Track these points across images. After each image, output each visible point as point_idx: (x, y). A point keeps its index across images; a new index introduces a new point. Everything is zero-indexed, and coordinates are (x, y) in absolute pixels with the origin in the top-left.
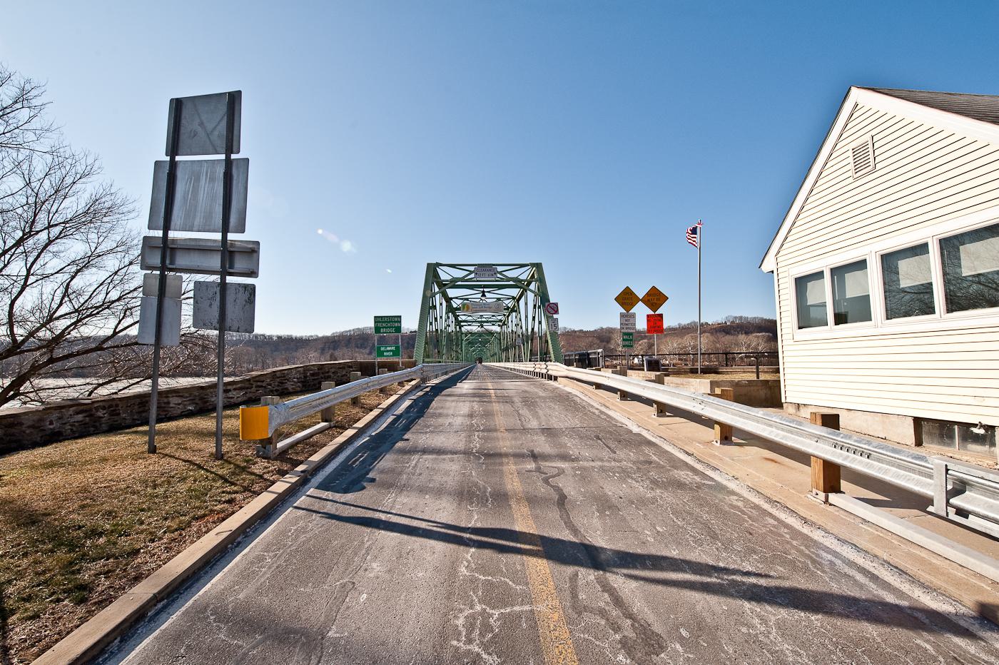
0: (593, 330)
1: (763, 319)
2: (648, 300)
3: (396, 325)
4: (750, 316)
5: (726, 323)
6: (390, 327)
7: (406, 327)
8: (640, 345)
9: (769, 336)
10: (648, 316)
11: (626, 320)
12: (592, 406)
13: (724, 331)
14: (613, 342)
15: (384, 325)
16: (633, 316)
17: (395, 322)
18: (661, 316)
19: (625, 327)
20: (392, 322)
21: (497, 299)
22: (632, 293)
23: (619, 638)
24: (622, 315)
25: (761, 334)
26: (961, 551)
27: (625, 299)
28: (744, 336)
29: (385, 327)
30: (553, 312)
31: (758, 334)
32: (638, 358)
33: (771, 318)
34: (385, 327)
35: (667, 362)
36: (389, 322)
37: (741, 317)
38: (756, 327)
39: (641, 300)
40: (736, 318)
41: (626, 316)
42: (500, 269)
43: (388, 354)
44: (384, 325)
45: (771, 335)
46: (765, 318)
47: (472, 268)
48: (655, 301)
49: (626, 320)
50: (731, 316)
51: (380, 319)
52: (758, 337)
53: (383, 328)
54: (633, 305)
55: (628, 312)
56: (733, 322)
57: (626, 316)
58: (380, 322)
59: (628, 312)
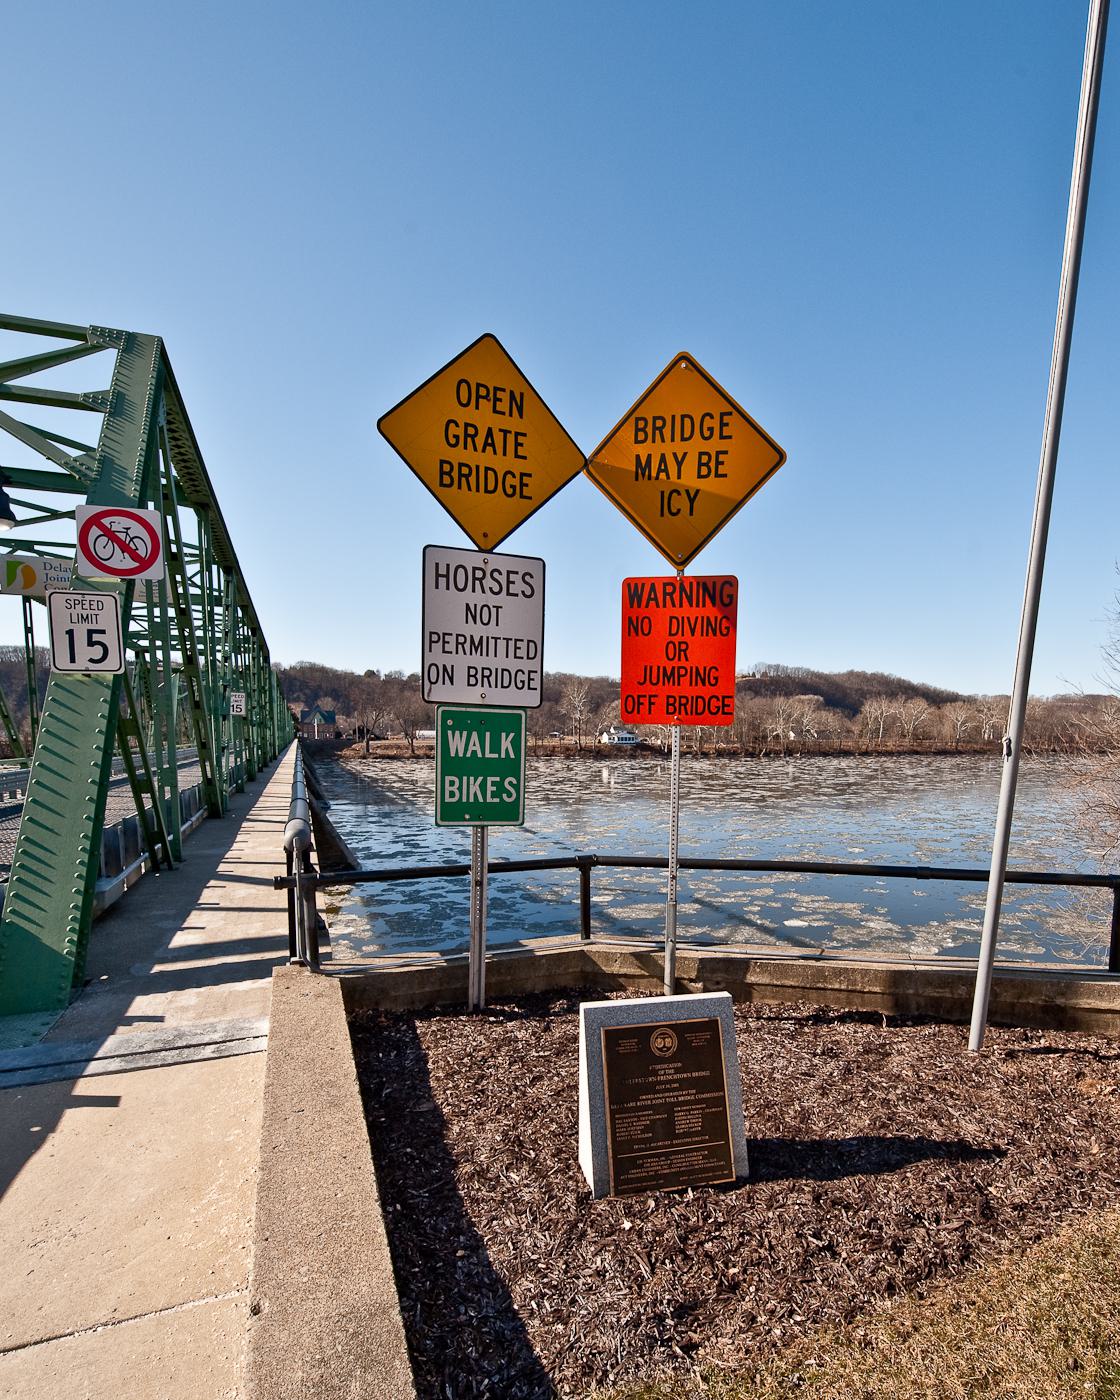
0: (360, 671)
1: (808, 672)
2: (642, 468)
4: (790, 666)
5: (754, 675)
7: (1037, 695)
8: (614, 709)
9: (818, 701)
10: (636, 593)
11: (471, 613)
13: (750, 689)
14: (565, 701)
16: (531, 578)
18: (722, 593)
19: (461, 662)
22: (521, 398)
24: (438, 571)
25: (807, 697)
28: (782, 698)
31: (803, 697)
32: (608, 732)
33: (820, 671)
35: (659, 742)
37: (778, 666)
38: (797, 683)
39: (586, 464)
40: (770, 666)
41: (477, 578)
45: (821, 699)
46: (812, 669)
48: (689, 479)
49: (471, 613)
50: (763, 664)
52: (803, 702)
55: (487, 545)
56: (764, 674)
57: (477, 578)
59: (487, 545)
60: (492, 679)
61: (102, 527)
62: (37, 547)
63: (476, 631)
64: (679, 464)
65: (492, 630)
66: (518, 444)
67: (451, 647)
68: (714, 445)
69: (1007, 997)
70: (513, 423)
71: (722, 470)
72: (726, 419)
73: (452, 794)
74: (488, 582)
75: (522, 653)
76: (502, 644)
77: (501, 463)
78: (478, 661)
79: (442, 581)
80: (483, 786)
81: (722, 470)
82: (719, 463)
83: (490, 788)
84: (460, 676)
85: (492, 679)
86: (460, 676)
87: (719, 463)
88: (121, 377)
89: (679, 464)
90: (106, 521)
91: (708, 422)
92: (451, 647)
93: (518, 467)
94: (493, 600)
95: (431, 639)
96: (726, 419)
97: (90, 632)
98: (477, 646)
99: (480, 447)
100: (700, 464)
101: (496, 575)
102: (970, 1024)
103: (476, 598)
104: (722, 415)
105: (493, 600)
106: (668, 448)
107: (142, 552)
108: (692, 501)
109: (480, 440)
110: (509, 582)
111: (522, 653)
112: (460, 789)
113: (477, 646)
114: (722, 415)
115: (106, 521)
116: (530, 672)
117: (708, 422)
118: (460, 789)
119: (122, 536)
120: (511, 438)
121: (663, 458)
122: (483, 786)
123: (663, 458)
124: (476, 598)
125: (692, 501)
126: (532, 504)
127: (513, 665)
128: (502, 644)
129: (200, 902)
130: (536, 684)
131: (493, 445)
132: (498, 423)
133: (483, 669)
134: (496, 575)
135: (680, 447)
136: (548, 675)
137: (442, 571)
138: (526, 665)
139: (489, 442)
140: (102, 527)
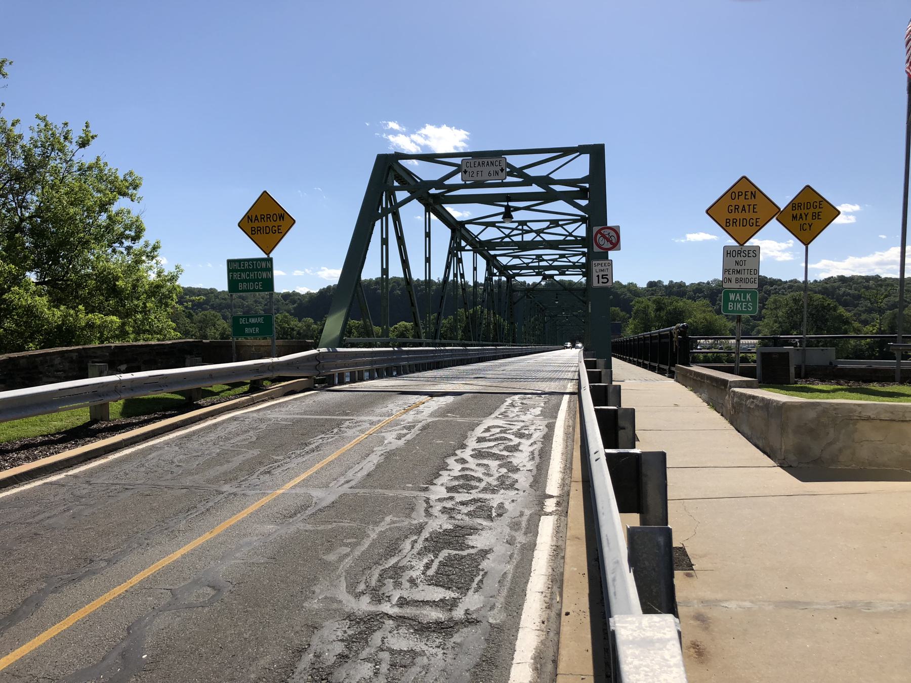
3: (264, 275)
6: (254, 281)
11: (737, 263)
12: (527, 208)
15: (243, 276)
17: (262, 270)
19: (734, 277)
20: (257, 270)
21: (552, 222)
23: (569, 628)
24: (728, 252)
26: (797, 396)
27: (736, 208)
29: (246, 281)
30: (607, 245)
34: (246, 281)
36: (253, 270)
41: (739, 253)
42: (511, 159)
43: (252, 330)
44: (243, 276)
47: (458, 161)
49: (737, 263)
51: (236, 266)
53: (243, 281)
54: (757, 226)
58: (237, 271)
59: (742, 245)
60: (738, 223)
61: (601, 234)
62: (497, 224)
63: (739, 268)
64: (806, 216)
65: (743, 267)
66: (754, 208)
67: (731, 273)
68: (817, 210)
69: (621, 423)
70: (752, 202)
71: (820, 217)
72: (821, 203)
73: (731, 308)
74: (742, 254)
75: (752, 273)
76: (746, 271)
77: (747, 215)
78: (739, 276)
79: (729, 255)
80: (741, 306)
81: (820, 217)
82: (819, 215)
83: (744, 306)
84: (733, 280)
85: (738, 223)
86: (733, 280)
87: (819, 215)
88: (236, 276)
89: (806, 216)
90: (602, 232)
91: (815, 204)
92: (731, 273)
93: (755, 216)
94: (743, 259)
95: (725, 271)
96: (821, 203)
97: (603, 275)
98: (738, 272)
99: (740, 211)
100: (813, 216)
101: (745, 255)
102: (728, 381)
103: (739, 259)
104: (820, 202)
105: (743, 259)
106: (802, 212)
107: (614, 241)
108: (810, 226)
109: (740, 210)
110: (748, 253)
111: (752, 273)
112: (733, 306)
113: (738, 272)
114: (820, 202)
115: (602, 232)
116: (756, 219)
117: (815, 204)
118: (733, 306)
119: (607, 236)
120: (751, 207)
121: (801, 215)
122: (741, 306)
123: (801, 215)
124: (739, 259)
125: (810, 226)
126: (759, 227)
127: (749, 277)
128: (746, 271)
129: (431, 214)
130: (757, 282)
131: (745, 210)
132: (746, 203)
133: (733, 219)
134: (745, 255)
135: (806, 211)
136: (761, 276)
137: (729, 252)
138: (754, 276)
139: (744, 209)
140: (601, 234)
